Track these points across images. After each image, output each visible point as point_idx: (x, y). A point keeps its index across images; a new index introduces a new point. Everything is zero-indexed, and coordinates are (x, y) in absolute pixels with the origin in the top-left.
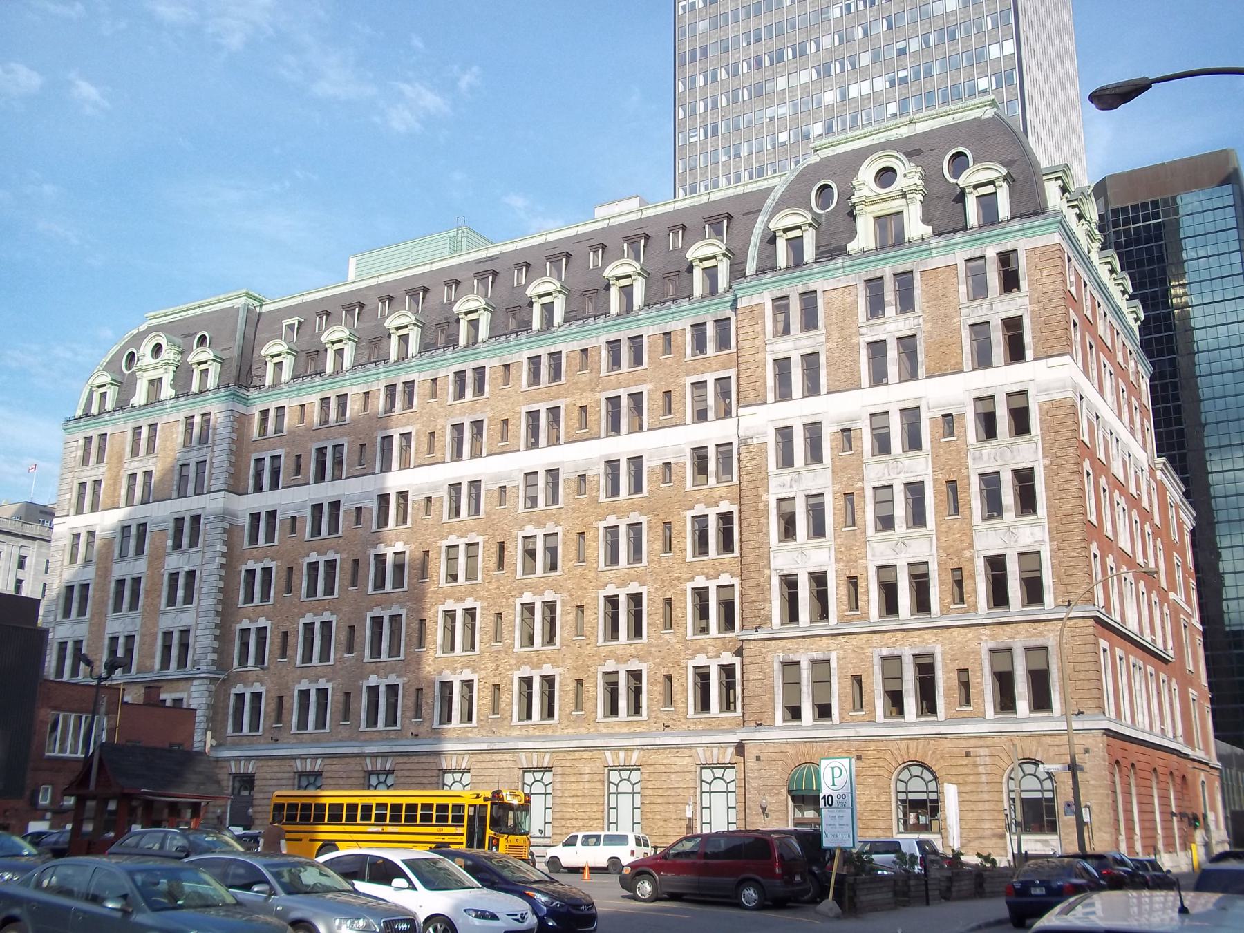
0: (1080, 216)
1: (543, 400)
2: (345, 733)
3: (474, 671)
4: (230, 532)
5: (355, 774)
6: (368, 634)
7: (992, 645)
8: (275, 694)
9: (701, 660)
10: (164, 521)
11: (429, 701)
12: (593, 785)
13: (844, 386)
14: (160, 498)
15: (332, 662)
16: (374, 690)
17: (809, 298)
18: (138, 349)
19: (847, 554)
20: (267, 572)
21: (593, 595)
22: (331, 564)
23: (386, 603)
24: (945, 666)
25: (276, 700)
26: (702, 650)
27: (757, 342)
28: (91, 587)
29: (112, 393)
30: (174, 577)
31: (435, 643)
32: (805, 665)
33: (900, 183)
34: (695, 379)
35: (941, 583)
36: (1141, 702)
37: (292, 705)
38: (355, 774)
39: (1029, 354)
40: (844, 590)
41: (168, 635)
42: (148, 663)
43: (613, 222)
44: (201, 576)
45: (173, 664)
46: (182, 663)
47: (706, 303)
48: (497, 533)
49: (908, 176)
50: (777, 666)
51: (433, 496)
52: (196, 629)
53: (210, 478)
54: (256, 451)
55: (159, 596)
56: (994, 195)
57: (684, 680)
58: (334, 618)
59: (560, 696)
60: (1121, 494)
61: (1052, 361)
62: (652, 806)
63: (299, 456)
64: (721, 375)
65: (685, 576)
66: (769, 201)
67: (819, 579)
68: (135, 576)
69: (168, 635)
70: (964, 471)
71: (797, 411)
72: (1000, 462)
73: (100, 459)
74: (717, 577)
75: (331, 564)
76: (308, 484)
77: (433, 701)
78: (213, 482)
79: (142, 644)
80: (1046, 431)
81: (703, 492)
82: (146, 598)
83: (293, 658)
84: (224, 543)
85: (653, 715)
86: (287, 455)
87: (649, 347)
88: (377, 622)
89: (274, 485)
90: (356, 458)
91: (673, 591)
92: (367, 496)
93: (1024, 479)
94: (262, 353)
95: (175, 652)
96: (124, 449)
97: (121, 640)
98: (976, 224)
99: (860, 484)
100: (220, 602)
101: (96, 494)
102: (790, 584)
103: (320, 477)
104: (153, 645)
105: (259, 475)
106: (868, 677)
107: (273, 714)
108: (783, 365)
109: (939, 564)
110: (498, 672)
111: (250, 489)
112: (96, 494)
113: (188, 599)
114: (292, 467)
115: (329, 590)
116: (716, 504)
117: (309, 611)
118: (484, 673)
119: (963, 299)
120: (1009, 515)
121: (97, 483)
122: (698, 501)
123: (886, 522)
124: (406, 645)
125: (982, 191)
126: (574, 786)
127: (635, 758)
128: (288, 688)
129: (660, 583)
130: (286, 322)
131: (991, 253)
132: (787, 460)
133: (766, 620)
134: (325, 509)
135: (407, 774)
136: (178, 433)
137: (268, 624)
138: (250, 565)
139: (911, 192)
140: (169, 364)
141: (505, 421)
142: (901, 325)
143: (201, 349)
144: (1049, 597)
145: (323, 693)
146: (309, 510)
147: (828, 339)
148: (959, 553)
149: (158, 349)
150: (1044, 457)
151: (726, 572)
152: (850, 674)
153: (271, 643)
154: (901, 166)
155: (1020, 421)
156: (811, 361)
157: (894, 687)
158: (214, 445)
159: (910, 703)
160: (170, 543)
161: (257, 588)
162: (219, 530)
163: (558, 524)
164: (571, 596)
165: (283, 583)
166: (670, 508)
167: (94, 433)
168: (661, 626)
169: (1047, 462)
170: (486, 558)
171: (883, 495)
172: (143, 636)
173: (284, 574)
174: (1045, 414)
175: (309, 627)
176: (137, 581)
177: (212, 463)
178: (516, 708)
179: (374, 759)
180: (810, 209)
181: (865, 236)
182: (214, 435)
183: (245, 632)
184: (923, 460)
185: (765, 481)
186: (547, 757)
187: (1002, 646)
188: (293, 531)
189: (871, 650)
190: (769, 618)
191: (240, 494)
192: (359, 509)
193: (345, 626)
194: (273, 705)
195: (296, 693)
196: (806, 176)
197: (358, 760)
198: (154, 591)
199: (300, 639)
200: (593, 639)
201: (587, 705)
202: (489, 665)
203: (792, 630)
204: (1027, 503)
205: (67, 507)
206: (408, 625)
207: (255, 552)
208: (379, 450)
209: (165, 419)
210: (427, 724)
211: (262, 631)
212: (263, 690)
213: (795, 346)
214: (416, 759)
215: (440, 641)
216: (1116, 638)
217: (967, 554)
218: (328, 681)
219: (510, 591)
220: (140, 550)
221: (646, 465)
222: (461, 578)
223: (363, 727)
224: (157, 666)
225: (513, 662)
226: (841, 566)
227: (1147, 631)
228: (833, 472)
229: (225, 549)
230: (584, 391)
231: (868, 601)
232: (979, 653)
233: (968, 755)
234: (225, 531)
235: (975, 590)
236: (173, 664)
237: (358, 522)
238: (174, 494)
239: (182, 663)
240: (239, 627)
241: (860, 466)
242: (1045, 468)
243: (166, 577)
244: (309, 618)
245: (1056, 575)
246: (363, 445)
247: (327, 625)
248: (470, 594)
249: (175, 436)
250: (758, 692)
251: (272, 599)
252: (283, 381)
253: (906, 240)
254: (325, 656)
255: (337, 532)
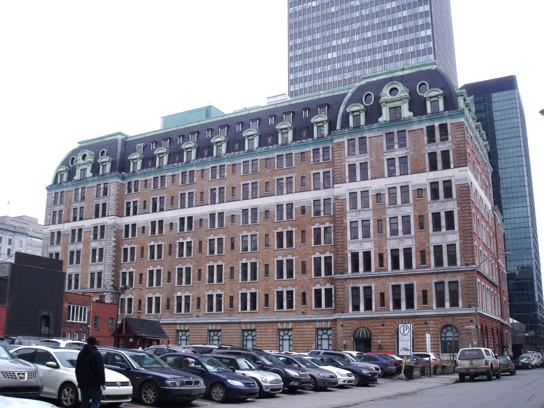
0: (470, 110)
1: (250, 179)
2: (168, 315)
3: (222, 290)
4: (117, 232)
5: (173, 331)
6: (176, 275)
7: (436, 281)
8: (138, 299)
9: (318, 287)
10: (90, 228)
11: (203, 302)
12: (273, 336)
13: (377, 176)
14: (87, 218)
15: (161, 286)
16: (179, 298)
17: (363, 140)
18: (77, 156)
19: (379, 245)
20: (133, 249)
21: (272, 260)
22: (159, 246)
23: (184, 262)
24: (417, 289)
25: (138, 301)
26: (318, 283)
27: (342, 158)
28: (60, 254)
29: (65, 176)
30: (94, 251)
31: (205, 279)
32: (361, 289)
33: (399, 95)
34: (315, 172)
35: (417, 256)
36: (489, 302)
37: (145, 303)
38: (173, 331)
39: (452, 166)
40: (377, 259)
41: (92, 274)
42: (85, 285)
43: (278, 106)
44: (106, 251)
45: (95, 286)
46: (99, 286)
47: (320, 141)
48: (231, 234)
49: (403, 92)
50: (350, 289)
51: (204, 218)
52: (105, 272)
53: (108, 210)
54: (127, 199)
55: (88, 258)
56: (437, 102)
57: (311, 295)
58: (162, 268)
59: (259, 301)
60: (484, 221)
61: (461, 169)
62: (297, 344)
63: (145, 202)
64: (326, 170)
65: (311, 253)
66: (345, 100)
67: (367, 255)
68: (78, 250)
69: (92, 274)
70: (426, 212)
71: (358, 186)
72: (440, 208)
73: (61, 203)
74: (325, 253)
75: (159, 246)
76: (149, 213)
77: (205, 303)
78: (109, 212)
79: (82, 278)
80: (459, 196)
81: (318, 219)
82: (83, 259)
83: (145, 284)
84: (115, 237)
85: (298, 308)
86: (140, 201)
87: (295, 158)
88: (180, 270)
89: (135, 213)
90: (170, 202)
91: (306, 258)
92: (175, 218)
93: (450, 215)
94: (129, 158)
95: (96, 281)
96: (72, 198)
97: (73, 276)
98: (430, 113)
99: (384, 216)
100: (114, 261)
101: (60, 215)
102: (355, 255)
103: (154, 210)
104: (86, 278)
105: (128, 209)
106: (387, 293)
107: (137, 307)
108: (352, 167)
109: (416, 249)
110: (232, 291)
111: (125, 215)
112: (60, 215)
113: (101, 260)
114: (142, 206)
115: (159, 257)
116: (324, 223)
117: (151, 265)
118: (226, 291)
119: (426, 142)
120: (444, 230)
121: (61, 211)
122: (316, 222)
123: (394, 232)
124: (193, 280)
125: (433, 99)
126: (265, 336)
127: (290, 326)
128: (143, 296)
129: (301, 255)
130: (138, 145)
131: (437, 124)
132: (354, 207)
133: (345, 271)
134: (157, 224)
135: (194, 331)
136: (94, 191)
137: (134, 270)
138: (126, 246)
139: (404, 98)
140: (90, 163)
141: (233, 188)
142: (401, 152)
143: (103, 157)
144: (459, 263)
145: (158, 299)
146: (150, 224)
147: (371, 157)
148: (424, 244)
149: (84, 157)
150: (458, 206)
151: (328, 251)
152: (379, 292)
153: (136, 278)
154: (400, 87)
155: (448, 194)
156: (364, 166)
157: (397, 297)
158: (109, 196)
159: (403, 304)
160: (92, 237)
161: (129, 256)
162: (113, 232)
163: (257, 231)
164: (263, 260)
165: (140, 254)
166: (304, 225)
167: (59, 191)
168: (301, 273)
169: (459, 209)
170: (226, 245)
171: (393, 221)
172: (82, 274)
173: (140, 250)
174: (458, 191)
175: (151, 272)
176: (78, 252)
177: (109, 204)
178: (240, 306)
179: (180, 326)
180: (362, 103)
181: (385, 116)
182: (110, 192)
183: (124, 274)
184: (410, 207)
185: (345, 214)
186: (254, 325)
187: (440, 281)
188: (143, 232)
189: (388, 283)
190: (347, 270)
191: (120, 217)
192: (171, 224)
193: (166, 272)
194: (137, 303)
195: (147, 299)
196: (361, 90)
197: (173, 326)
198: (86, 256)
199: (148, 277)
200: (272, 278)
201: (270, 304)
202: (228, 288)
203: (356, 275)
204: (450, 226)
205: (49, 221)
206: (193, 272)
207: (127, 241)
208: (179, 199)
209: (89, 185)
210: (202, 312)
211: (131, 273)
212: (132, 297)
213: (357, 160)
214: (198, 326)
215: (207, 278)
216: (482, 278)
217: (427, 245)
218: (160, 294)
219: (237, 258)
220: (58, 242)
221: (137, 226)
222: (216, 253)
223: (175, 313)
224: (89, 286)
225: (239, 287)
226: (377, 249)
227: (491, 275)
228: (373, 211)
229: (115, 239)
230: (267, 176)
231: (387, 263)
232: (431, 284)
233: (426, 323)
234: (115, 232)
235: (430, 259)
236: (95, 286)
237: (171, 229)
238: (94, 217)
239: (99, 286)
240: (122, 271)
241: (384, 209)
242: (458, 211)
243: (91, 251)
244: (151, 268)
245: (461, 253)
246: (172, 197)
247: (159, 271)
248: (220, 259)
249: (93, 192)
250: (342, 299)
251: (135, 260)
252: (138, 170)
253: (403, 118)
254: (158, 283)
255: (162, 233)
